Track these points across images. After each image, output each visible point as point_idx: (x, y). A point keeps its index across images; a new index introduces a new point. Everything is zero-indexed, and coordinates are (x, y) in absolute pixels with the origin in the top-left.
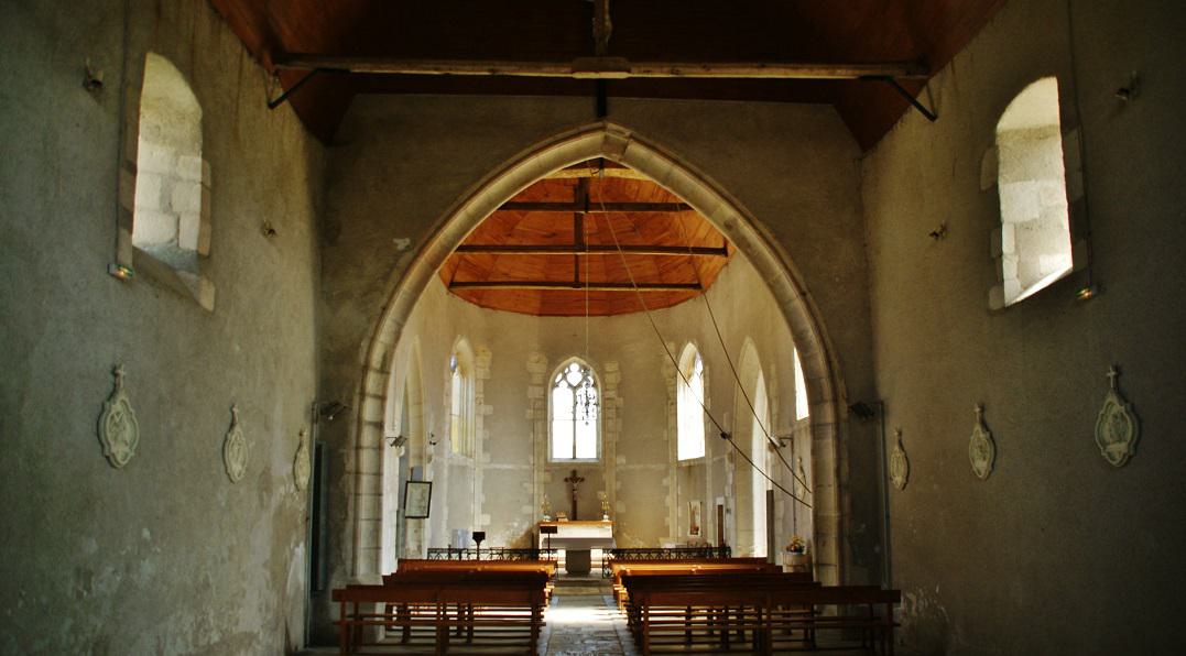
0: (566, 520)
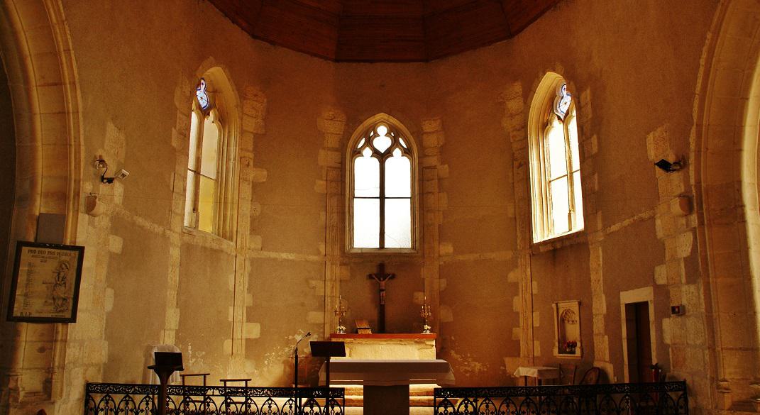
0: (369, 332)
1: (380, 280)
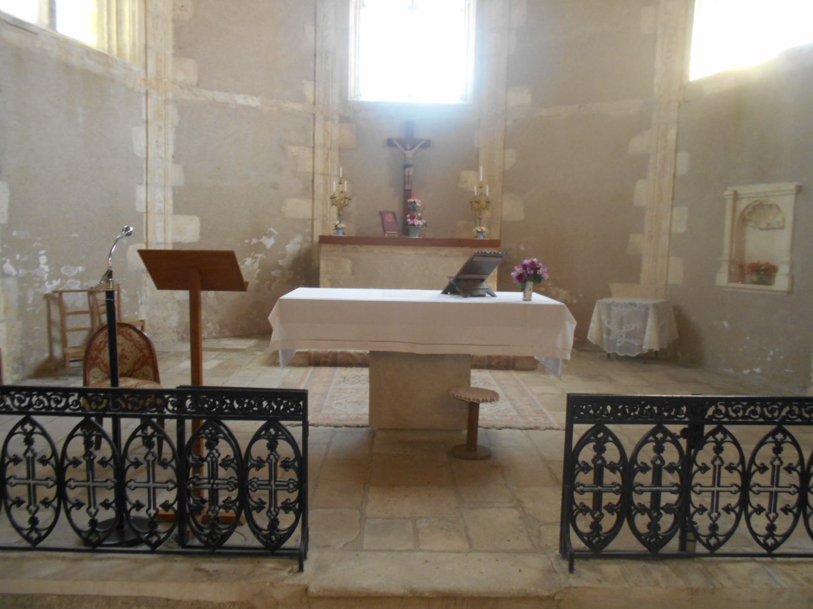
1: (406, 149)
